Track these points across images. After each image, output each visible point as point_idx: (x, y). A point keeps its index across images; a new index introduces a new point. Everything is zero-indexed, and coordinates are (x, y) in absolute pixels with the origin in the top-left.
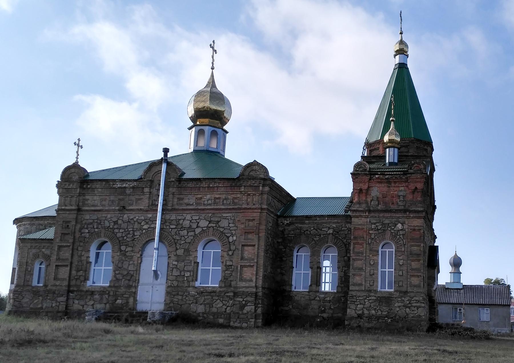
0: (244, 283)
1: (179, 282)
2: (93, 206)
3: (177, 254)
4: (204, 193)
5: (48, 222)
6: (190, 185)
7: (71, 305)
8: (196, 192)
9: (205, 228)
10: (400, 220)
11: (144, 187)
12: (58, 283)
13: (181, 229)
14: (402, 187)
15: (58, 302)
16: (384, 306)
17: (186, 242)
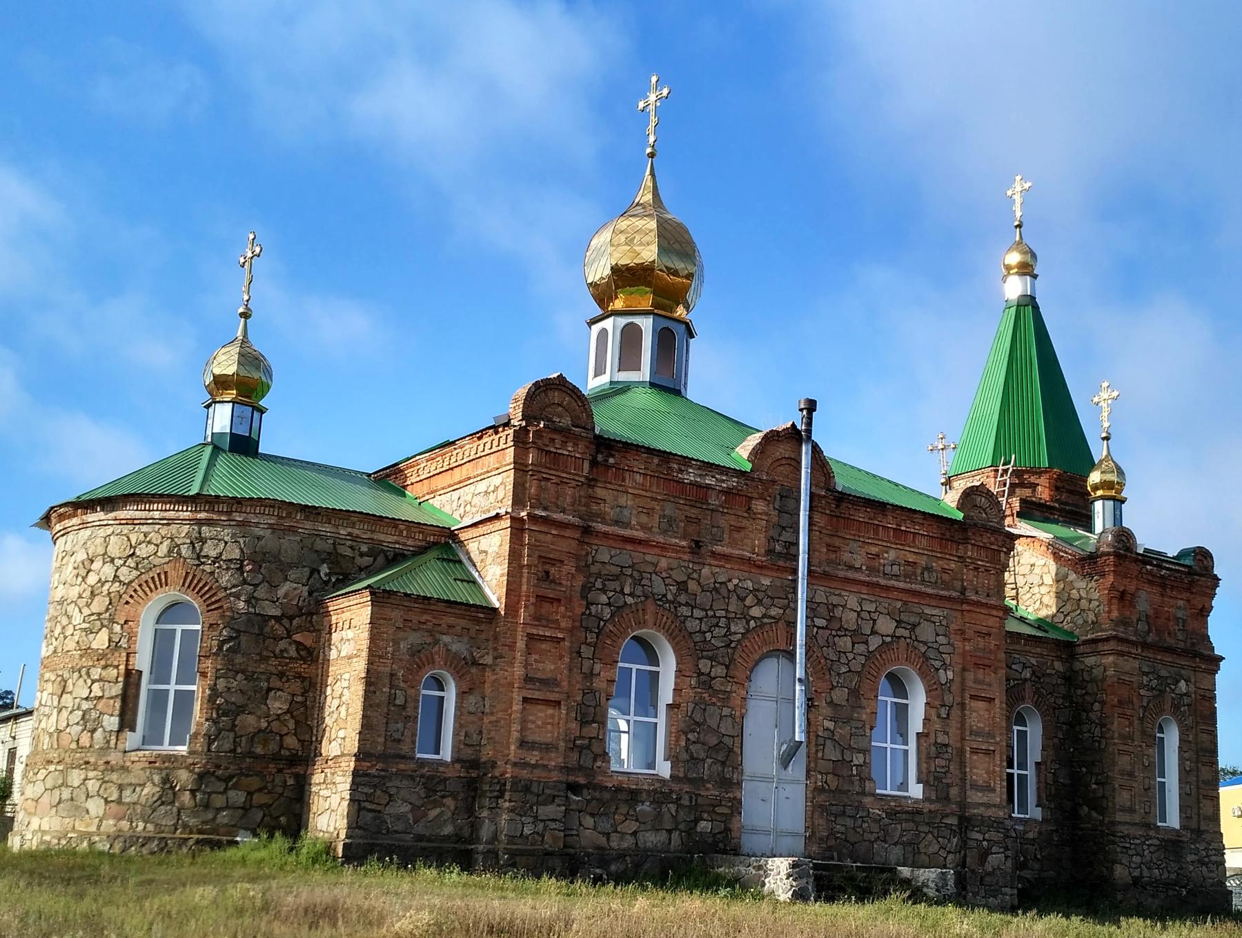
0: (980, 794)
1: (840, 779)
2: (616, 522)
3: (832, 701)
4: (884, 544)
5: (349, 530)
6: (861, 516)
7: (574, 832)
8: (869, 538)
9: (889, 639)
10: (1183, 672)
11: (755, 495)
12: (533, 757)
13: (839, 633)
14: (1181, 599)
15: (542, 821)
16: (1172, 861)
17: (850, 671)
